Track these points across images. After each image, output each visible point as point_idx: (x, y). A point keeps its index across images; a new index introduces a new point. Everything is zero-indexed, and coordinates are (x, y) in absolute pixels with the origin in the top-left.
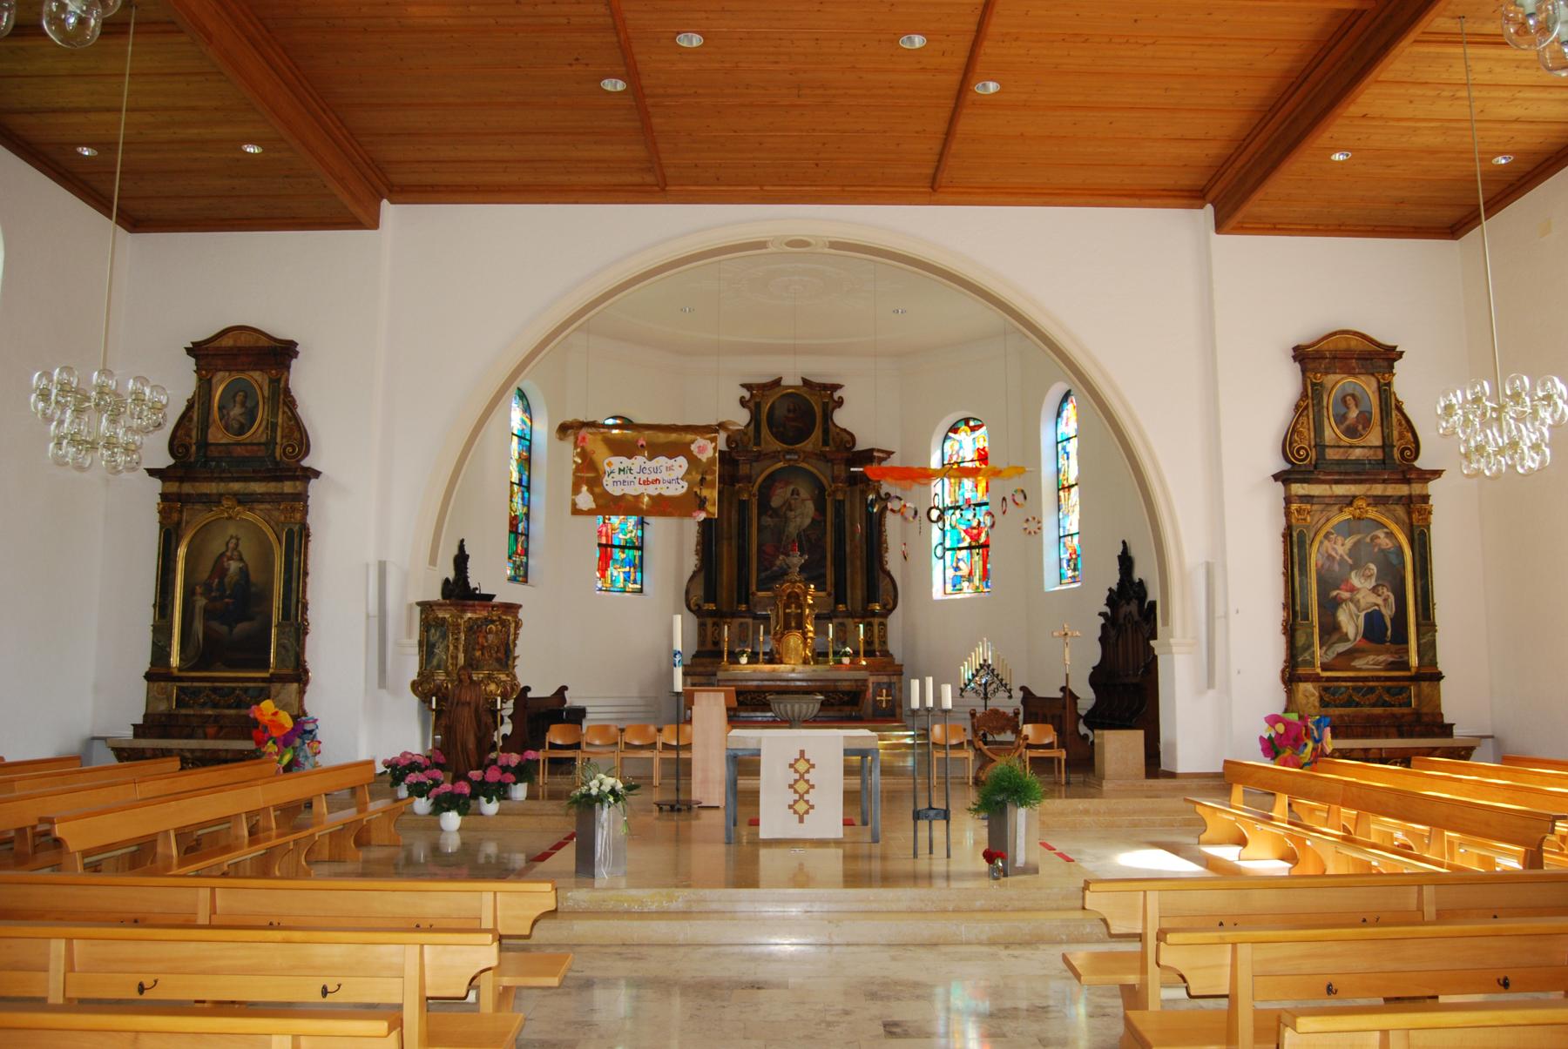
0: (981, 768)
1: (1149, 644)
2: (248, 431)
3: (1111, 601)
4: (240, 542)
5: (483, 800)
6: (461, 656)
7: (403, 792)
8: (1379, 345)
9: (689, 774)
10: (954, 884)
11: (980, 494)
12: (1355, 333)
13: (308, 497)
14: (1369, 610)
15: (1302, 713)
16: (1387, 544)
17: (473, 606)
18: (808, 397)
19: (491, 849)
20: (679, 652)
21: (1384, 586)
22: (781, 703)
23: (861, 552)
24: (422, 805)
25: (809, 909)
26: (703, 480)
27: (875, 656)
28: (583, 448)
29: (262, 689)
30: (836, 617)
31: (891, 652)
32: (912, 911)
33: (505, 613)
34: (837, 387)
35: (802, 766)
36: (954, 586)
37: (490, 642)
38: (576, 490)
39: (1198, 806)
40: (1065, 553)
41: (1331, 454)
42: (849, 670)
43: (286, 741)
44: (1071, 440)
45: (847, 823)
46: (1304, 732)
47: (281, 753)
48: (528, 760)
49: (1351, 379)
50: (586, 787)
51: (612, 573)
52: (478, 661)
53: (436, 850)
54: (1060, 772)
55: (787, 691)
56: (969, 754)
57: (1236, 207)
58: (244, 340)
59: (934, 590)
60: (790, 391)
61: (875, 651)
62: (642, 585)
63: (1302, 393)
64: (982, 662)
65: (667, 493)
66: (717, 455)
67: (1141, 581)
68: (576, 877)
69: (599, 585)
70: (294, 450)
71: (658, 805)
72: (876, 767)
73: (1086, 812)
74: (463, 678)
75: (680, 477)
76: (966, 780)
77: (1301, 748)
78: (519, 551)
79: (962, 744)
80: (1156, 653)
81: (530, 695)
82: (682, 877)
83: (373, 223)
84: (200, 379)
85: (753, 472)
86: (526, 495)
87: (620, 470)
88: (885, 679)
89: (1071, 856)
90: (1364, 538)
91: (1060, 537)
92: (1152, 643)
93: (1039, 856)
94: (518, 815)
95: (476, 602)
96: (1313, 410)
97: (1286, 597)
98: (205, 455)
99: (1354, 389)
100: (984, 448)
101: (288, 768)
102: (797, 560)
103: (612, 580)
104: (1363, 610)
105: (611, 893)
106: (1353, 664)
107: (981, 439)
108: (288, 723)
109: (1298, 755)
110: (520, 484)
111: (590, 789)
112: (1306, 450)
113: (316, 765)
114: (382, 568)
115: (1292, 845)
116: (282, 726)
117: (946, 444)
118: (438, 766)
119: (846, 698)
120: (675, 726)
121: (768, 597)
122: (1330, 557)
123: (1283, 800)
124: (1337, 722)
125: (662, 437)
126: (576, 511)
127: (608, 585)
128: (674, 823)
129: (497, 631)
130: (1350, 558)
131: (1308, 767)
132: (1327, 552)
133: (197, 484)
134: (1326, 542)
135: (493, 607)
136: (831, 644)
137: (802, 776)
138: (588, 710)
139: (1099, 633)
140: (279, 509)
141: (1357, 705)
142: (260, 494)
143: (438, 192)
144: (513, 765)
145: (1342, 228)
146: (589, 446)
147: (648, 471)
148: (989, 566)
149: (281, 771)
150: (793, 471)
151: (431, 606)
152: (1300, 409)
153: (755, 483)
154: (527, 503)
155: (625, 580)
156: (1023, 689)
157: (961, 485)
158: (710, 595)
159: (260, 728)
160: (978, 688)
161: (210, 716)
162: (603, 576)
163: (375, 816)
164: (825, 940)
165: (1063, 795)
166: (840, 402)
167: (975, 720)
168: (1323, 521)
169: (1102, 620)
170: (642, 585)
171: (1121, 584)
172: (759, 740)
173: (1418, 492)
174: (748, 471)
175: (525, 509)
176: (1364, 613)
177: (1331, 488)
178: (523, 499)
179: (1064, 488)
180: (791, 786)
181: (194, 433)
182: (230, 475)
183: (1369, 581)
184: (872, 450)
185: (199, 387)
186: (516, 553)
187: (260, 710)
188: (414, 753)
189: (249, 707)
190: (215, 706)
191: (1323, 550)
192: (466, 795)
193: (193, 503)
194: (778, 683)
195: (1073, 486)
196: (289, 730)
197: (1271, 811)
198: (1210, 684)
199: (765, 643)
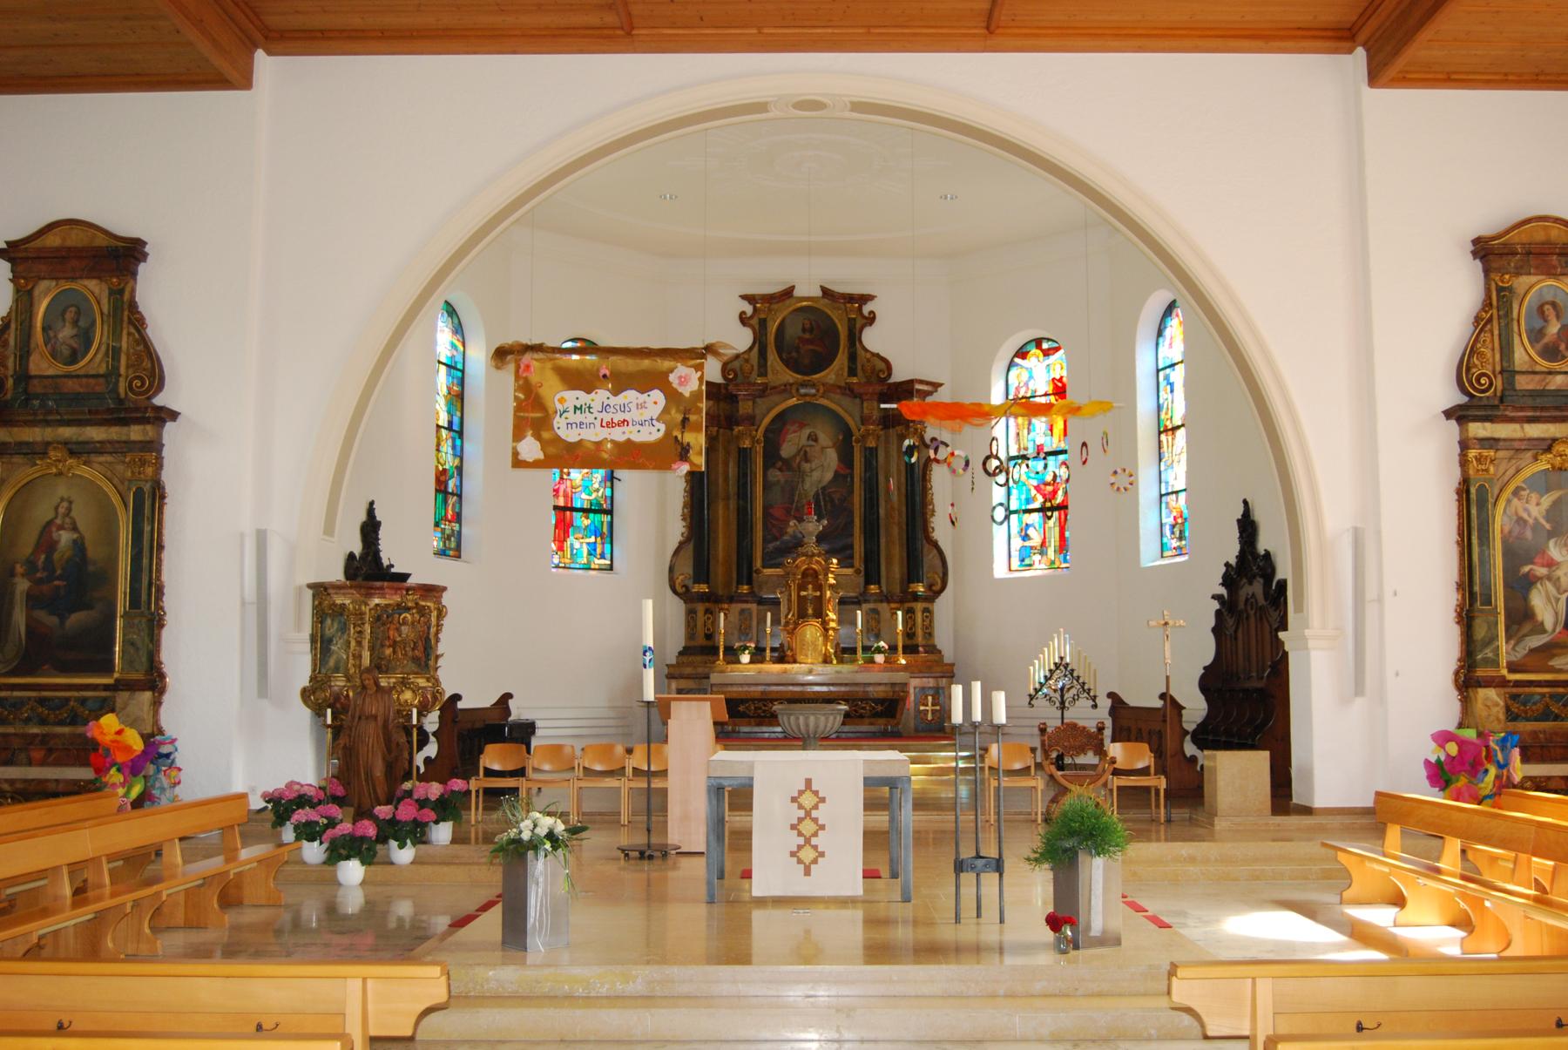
0: (1054, 800)
1: (1277, 636)
2: (84, 357)
3: (1227, 581)
4: (73, 506)
5: (393, 844)
6: (366, 655)
7: (288, 834)
9: (664, 809)
10: (1009, 960)
11: (1056, 439)
12: (1557, 220)
13: (163, 445)
15: (1481, 729)
17: (382, 588)
18: (829, 312)
19: (404, 909)
20: (650, 648)
22: (791, 714)
23: (900, 514)
24: (313, 852)
25: (812, 993)
26: (685, 421)
27: (918, 652)
28: (526, 380)
29: (105, 700)
30: (866, 601)
31: (938, 647)
32: (946, 997)
33: (424, 598)
34: (865, 299)
35: (808, 800)
36: (1023, 560)
37: (404, 636)
38: (518, 436)
39: (1339, 853)
40: (1168, 517)
41: (1523, 383)
42: (884, 671)
43: (134, 768)
44: (1176, 367)
45: (869, 875)
46: (1484, 754)
47: (126, 783)
48: (452, 791)
49: (1551, 282)
50: (515, 830)
51: (572, 545)
52: (389, 661)
53: (331, 910)
54: (1158, 806)
55: (803, 699)
56: (1039, 782)
57: (1396, 53)
58: (76, 239)
59: (996, 566)
60: (805, 303)
61: (917, 646)
62: (612, 560)
63: (1485, 301)
64: (1057, 660)
65: (637, 438)
66: (704, 387)
67: (1267, 555)
68: (503, 950)
69: (556, 560)
70: (143, 384)
71: (623, 851)
72: (906, 801)
73: (1192, 860)
74: (367, 684)
75: (654, 418)
76: (1033, 817)
77: (1480, 775)
78: (450, 517)
79: (1028, 768)
80: (1286, 648)
81: (460, 705)
82: (656, 951)
83: (243, 80)
84: (17, 290)
85: (757, 411)
86: (458, 442)
87: (575, 407)
88: (931, 682)
89: (1166, 920)
91: (1161, 496)
92: (1281, 635)
93: (1116, 924)
94: (440, 864)
95: (386, 584)
96: (1499, 323)
97: (1461, 574)
98: (25, 391)
99: (1555, 295)
100: (1062, 377)
101: (138, 804)
102: (813, 526)
103: (572, 554)
105: (547, 971)
106: (1551, 663)
107: (1057, 366)
108: (138, 745)
109: (1476, 785)
110: (450, 428)
111: (521, 832)
112: (1489, 377)
113: (175, 799)
114: (261, 538)
115: (1466, 907)
116: (128, 749)
117: (1011, 373)
118: (339, 801)
119: (879, 708)
120: (646, 745)
121: (778, 576)
122: (1521, 521)
123: (1454, 846)
124: (1529, 741)
125: (630, 365)
126: (518, 463)
127: (567, 561)
128: (644, 876)
129: (413, 623)
130: (1548, 521)
131: (1489, 801)
132: (1516, 513)
133: (16, 429)
134: (1515, 501)
135: (408, 590)
136: (860, 637)
137: (808, 814)
138: (538, 724)
139: (1212, 623)
140: (124, 462)
141: (1557, 718)
142: (99, 442)
143: (330, 38)
144: (433, 798)
145: (1542, 78)
146: (534, 378)
147: (612, 410)
148: (1067, 534)
149: (129, 807)
150: (808, 410)
151: (326, 589)
152: (1481, 323)
153: (759, 427)
154: (459, 454)
155: (590, 554)
156: (1111, 695)
157: (1031, 427)
158: (702, 571)
159: (100, 751)
160: (1052, 694)
161: (37, 735)
162: (561, 548)
163: (248, 867)
164: (836, 1036)
165: (1163, 837)
166: (871, 319)
167: (1046, 738)
168: (1511, 471)
169: (1216, 605)
170: (612, 560)
171: (1241, 557)
172: (751, 765)
174: (750, 411)
175: (457, 461)
177: (1522, 428)
178: (454, 447)
179: (1166, 430)
180: (793, 827)
181: (10, 363)
182: (59, 417)
184: (911, 382)
185: (16, 301)
186: (445, 518)
187: (100, 727)
188: (303, 782)
189: (86, 723)
190: (43, 722)
191: (1511, 511)
192: (371, 838)
193: (11, 454)
194: (791, 688)
195: (1178, 427)
196: (138, 753)
197: (1438, 859)
198: (1359, 690)
199: (773, 637)
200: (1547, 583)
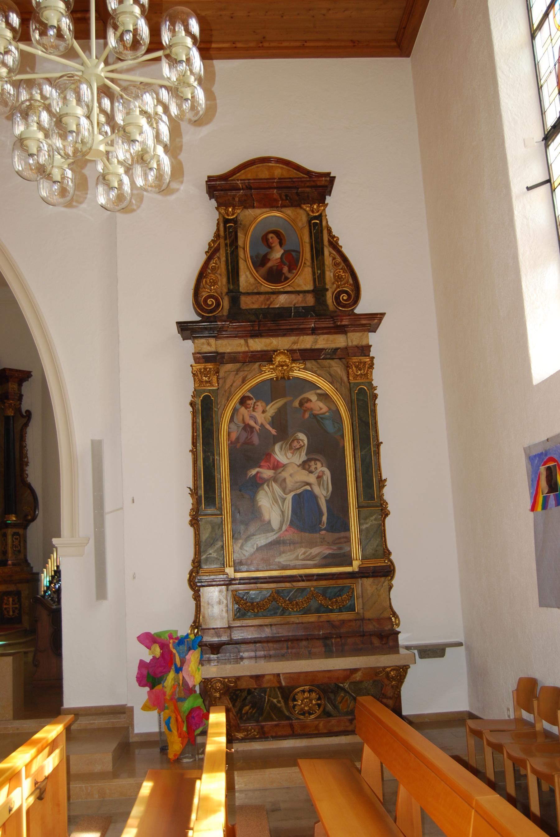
8: (308, 173)
14: (299, 491)
16: (321, 409)
21: (316, 460)
41: (247, 303)
64: (55, 569)
90: (292, 401)
104: (291, 491)
122: (248, 428)
134: (243, 410)
173: (355, 343)
176: (292, 494)
177: (246, 342)
183: (297, 454)
200: (273, 484)
